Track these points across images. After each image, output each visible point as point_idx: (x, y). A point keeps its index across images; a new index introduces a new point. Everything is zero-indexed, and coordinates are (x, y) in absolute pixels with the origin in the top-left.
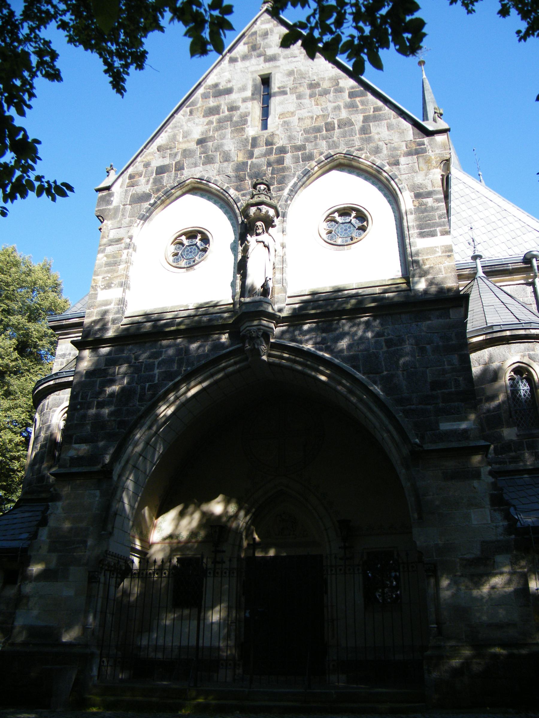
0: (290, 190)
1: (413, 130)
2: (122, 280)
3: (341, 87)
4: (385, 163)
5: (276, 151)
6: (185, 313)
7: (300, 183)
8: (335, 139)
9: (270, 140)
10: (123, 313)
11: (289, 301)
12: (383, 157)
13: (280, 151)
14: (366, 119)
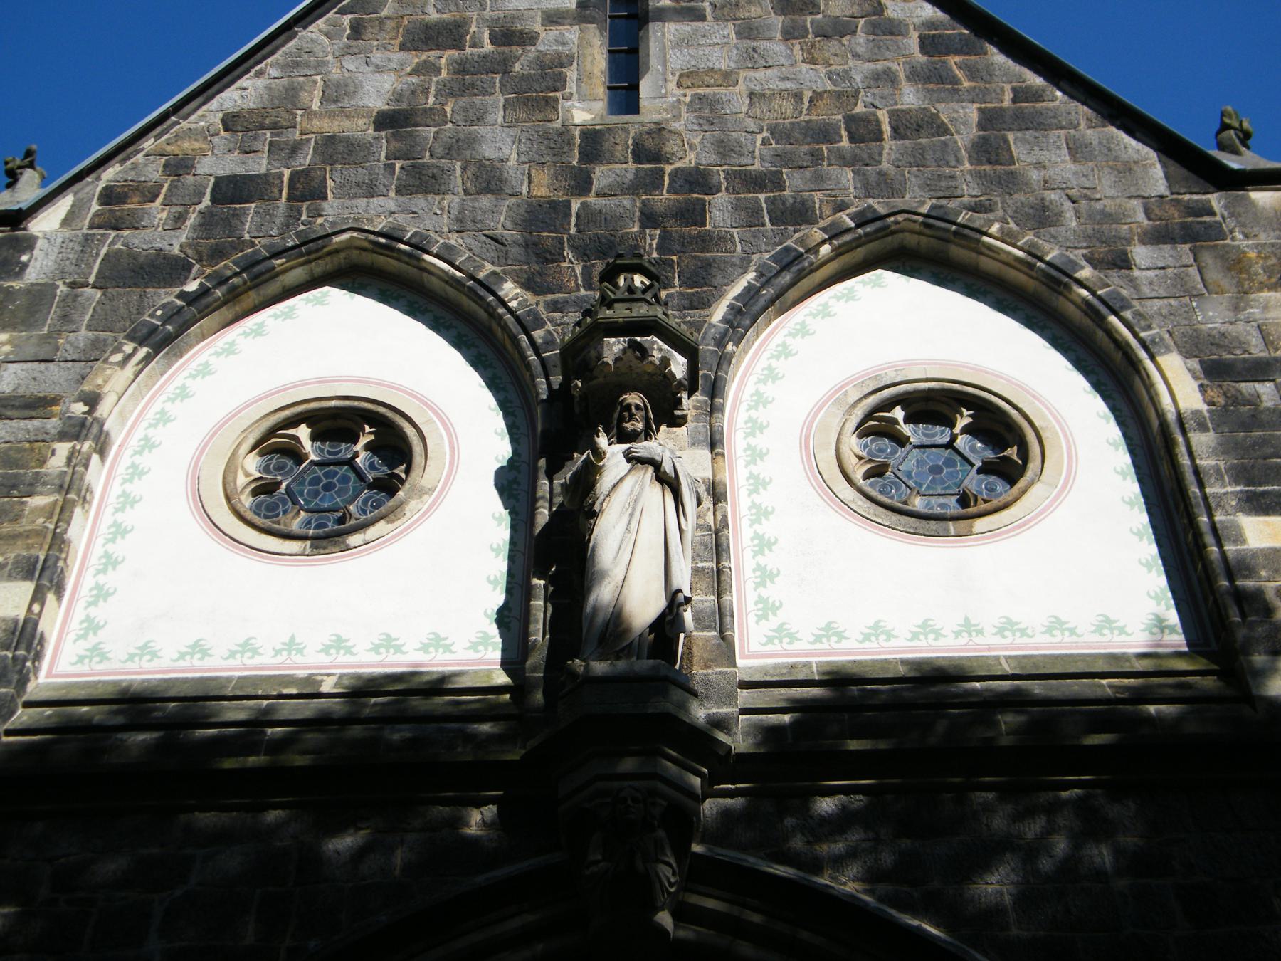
0: (731, 307)
1: (1164, 166)
2: (33, 552)
3: (891, 20)
4: (1077, 255)
5: (672, 181)
6: (308, 709)
7: (768, 292)
8: (885, 166)
9: (649, 144)
10: (23, 682)
11: (745, 697)
12: (1067, 239)
13: (691, 183)
14: (989, 119)
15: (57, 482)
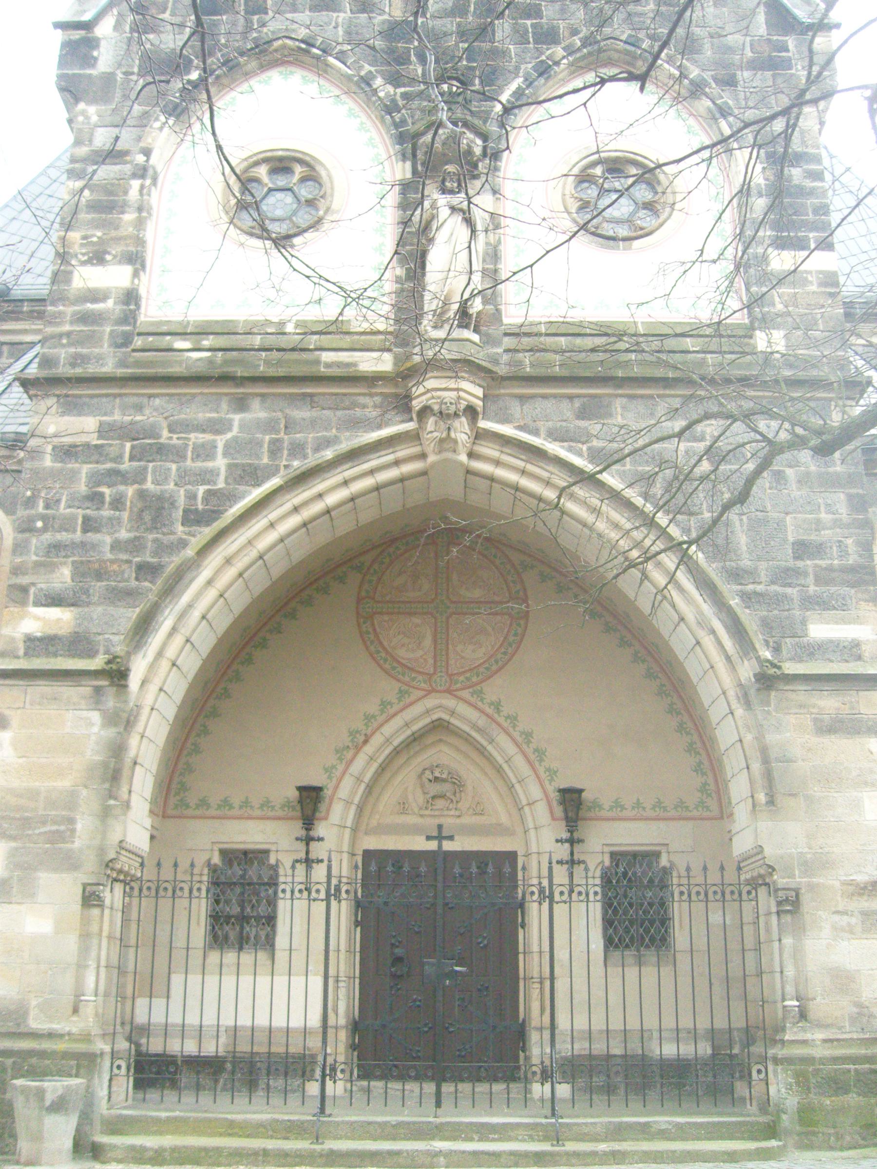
11: (508, 342)
15: (136, 205)
